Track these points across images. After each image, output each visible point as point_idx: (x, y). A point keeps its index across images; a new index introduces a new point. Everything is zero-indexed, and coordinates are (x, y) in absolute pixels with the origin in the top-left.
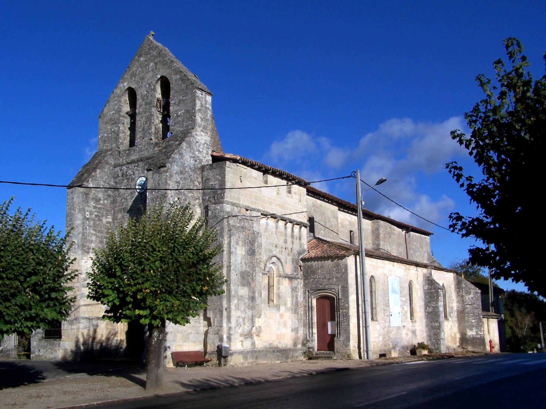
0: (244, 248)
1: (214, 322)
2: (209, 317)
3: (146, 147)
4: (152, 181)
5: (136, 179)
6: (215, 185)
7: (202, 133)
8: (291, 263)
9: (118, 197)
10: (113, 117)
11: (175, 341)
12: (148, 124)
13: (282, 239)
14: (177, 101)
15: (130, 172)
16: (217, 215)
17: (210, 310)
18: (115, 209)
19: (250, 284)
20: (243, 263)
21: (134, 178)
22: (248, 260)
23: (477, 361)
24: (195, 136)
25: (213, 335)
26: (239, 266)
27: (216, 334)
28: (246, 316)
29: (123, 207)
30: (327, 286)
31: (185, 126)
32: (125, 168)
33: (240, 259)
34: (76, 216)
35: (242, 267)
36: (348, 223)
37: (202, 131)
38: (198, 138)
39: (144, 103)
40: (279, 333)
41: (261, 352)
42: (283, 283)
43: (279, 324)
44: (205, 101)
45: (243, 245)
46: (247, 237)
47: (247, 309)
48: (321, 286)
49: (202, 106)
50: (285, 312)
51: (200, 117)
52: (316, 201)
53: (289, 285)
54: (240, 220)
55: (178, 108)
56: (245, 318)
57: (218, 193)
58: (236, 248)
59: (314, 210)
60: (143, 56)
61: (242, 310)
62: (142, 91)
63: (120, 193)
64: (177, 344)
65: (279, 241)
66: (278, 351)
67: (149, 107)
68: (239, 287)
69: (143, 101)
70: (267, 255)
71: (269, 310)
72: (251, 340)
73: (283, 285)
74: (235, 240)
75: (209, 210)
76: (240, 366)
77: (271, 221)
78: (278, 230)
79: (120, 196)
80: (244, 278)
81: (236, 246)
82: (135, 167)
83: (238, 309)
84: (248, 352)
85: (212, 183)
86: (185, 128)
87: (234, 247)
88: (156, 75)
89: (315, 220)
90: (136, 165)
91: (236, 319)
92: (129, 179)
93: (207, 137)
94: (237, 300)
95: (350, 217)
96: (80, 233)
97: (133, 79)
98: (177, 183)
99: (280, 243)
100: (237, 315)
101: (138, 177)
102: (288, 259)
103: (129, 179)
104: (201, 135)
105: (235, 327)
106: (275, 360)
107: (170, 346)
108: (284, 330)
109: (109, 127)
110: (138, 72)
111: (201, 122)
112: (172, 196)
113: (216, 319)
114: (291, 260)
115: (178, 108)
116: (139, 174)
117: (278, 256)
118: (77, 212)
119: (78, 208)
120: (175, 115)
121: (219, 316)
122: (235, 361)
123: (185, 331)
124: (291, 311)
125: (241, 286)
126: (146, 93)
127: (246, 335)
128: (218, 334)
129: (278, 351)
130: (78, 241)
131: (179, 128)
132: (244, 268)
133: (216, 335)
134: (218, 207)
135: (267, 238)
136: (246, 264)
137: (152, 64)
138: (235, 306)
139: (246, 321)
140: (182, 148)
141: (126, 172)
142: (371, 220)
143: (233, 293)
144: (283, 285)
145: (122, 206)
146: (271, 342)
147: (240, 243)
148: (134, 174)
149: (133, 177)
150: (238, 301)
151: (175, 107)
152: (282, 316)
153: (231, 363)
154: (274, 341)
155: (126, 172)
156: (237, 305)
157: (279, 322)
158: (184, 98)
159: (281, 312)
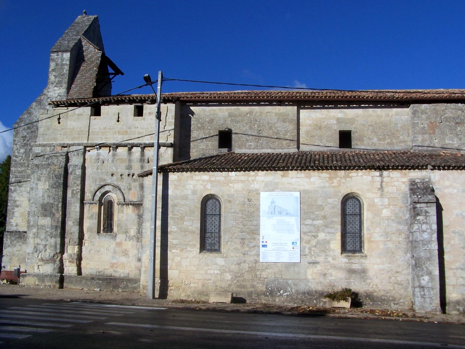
0: (47, 183)
7: (55, 88)
8: (138, 189)
11: (10, 263)
13: (124, 165)
19: (54, 214)
20: (46, 196)
22: (52, 193)
23: (35, 307)
24: (47, 93)
26: (40, 199)
28: (47, 243)
33: (41, 193)
35: (44, 199)
36: (335, 122)
37: (56, 86)
38: (50, 94)
40: (115, 261)
41: (72, 278)
42: (123, 211)
43: (115, 252)
44: (62, 59)
45: (46, 181)
46: (52, 172)
47: (49, 238)
49: (57, 65)
50: (126, 240)
51: (54, 75)
52: (204, 111)
53: (133, 212)
54: (48, 158)
56: (46, 245)
58: (37, 184)
59: (232, 121)
61: (43, 237)
64: (13, 265)
65: (117, 169)
66: (99, 279)
68: (40, 218)
70: (96, 185)
71: (99, 238)
72: (52, 265)
73: (123, 213)
74: (36, 177)
76: (32, 287)
77: (104, 151)
78: (117, 158)
80: (45, 210)
81: (37, 182)
83: (37, 237)
84: (46, 276)
87: (35, 183)
89: (234, 131)
91: (33, 246)
93: (61, 90)
94: (36, 229)
95: (342, 112)
98: (23, 137)
99: (119, 170)
100: (36, 242)
102: (132, 186)
104: (54, 90)
105: (33, 253)
106: (95, 288)
107: (4, 266)
108: (123, 259)
111: (55, 79)
112: (17, 149)
114: (138, 186)
117: (115, 183)
122: (25, 282)
123: (22, 255)
124: (135, 239)
125: (42, 217)
127: (47, 260)
129: (99, 279)
132: (46, 200)
135: (98, 169)
136: (49, 196)
138: (34, 234)
139: (47, 247)
140: (31, 108)
142: (408, 107)
143: (32, 223)
144: (123, 213)
146: (100, 270)
147: (43, 179)
150: (38, 229)
152: (119, 244)
153: (23, 284)
154: (107, 269)
156: (36, 233)
157: (115, 250)
159: (118, 240)
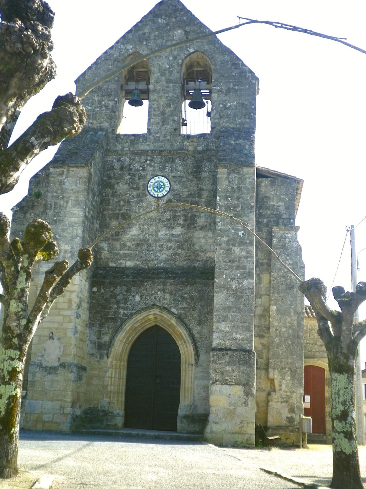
1: (280, 386)
2: (272, 378)
3: (168, 138)
4: (227, 183)
5: (149, 177)
6: (278, 206)
9: (112, 196)
10: (105, 87)
12: (172, 109)
14: (224, 88)
15: (137, 166)
16: (287, 245)
17: (274, 369)
18: (106, 212)
21: (145, 176)
25: (280, 404)
27: (284, 402)
29: (122, 212)
30: (317, 353)
31: (238, 123)
32: (128, 159)
34: (68, 209)
39: (163, 79)
48: (309, 353)
55: (225, 98)
57: (283, 217)
60: (163, 17)
62: (160, 63)
63: (116, 192)
67: (173, 86)
69: (161, 76)
75: (274, 236)
79: (116, 196)
82: (146, 161)
85: (273, 203)
86: (238, 126)
88: (187, 48)
90: (149, 158)
92: (134, 175)
96: (77, 236)
97: (145, 43)
101: (152, 175)
103: (134, 175)
109: (96, 99)
110: (152, 37)
113: (284, 381)
115: (225, 98)
116: (154, 171)
118: (70, 204)
119: (73, 198)
120: (221, 106)
121: (289, 378)
126: (168, 66)
128: (287, 402)
130: (72, 248)
131: (227, 124)
133: (284, 404)
134: (289, 235)
137: (179, 31)
141: (130, 165)
145: (120, 210)
148: (144, 169)
149: (143, 173)
151: (221, 96)
155: (130, 165)
158: (236, 87)
